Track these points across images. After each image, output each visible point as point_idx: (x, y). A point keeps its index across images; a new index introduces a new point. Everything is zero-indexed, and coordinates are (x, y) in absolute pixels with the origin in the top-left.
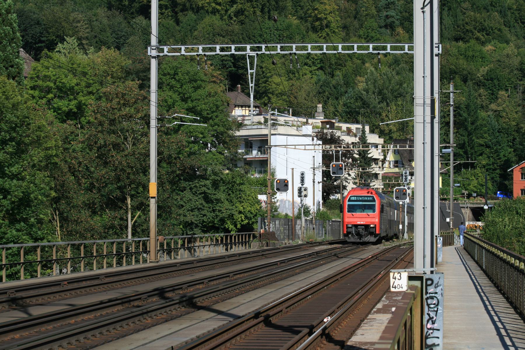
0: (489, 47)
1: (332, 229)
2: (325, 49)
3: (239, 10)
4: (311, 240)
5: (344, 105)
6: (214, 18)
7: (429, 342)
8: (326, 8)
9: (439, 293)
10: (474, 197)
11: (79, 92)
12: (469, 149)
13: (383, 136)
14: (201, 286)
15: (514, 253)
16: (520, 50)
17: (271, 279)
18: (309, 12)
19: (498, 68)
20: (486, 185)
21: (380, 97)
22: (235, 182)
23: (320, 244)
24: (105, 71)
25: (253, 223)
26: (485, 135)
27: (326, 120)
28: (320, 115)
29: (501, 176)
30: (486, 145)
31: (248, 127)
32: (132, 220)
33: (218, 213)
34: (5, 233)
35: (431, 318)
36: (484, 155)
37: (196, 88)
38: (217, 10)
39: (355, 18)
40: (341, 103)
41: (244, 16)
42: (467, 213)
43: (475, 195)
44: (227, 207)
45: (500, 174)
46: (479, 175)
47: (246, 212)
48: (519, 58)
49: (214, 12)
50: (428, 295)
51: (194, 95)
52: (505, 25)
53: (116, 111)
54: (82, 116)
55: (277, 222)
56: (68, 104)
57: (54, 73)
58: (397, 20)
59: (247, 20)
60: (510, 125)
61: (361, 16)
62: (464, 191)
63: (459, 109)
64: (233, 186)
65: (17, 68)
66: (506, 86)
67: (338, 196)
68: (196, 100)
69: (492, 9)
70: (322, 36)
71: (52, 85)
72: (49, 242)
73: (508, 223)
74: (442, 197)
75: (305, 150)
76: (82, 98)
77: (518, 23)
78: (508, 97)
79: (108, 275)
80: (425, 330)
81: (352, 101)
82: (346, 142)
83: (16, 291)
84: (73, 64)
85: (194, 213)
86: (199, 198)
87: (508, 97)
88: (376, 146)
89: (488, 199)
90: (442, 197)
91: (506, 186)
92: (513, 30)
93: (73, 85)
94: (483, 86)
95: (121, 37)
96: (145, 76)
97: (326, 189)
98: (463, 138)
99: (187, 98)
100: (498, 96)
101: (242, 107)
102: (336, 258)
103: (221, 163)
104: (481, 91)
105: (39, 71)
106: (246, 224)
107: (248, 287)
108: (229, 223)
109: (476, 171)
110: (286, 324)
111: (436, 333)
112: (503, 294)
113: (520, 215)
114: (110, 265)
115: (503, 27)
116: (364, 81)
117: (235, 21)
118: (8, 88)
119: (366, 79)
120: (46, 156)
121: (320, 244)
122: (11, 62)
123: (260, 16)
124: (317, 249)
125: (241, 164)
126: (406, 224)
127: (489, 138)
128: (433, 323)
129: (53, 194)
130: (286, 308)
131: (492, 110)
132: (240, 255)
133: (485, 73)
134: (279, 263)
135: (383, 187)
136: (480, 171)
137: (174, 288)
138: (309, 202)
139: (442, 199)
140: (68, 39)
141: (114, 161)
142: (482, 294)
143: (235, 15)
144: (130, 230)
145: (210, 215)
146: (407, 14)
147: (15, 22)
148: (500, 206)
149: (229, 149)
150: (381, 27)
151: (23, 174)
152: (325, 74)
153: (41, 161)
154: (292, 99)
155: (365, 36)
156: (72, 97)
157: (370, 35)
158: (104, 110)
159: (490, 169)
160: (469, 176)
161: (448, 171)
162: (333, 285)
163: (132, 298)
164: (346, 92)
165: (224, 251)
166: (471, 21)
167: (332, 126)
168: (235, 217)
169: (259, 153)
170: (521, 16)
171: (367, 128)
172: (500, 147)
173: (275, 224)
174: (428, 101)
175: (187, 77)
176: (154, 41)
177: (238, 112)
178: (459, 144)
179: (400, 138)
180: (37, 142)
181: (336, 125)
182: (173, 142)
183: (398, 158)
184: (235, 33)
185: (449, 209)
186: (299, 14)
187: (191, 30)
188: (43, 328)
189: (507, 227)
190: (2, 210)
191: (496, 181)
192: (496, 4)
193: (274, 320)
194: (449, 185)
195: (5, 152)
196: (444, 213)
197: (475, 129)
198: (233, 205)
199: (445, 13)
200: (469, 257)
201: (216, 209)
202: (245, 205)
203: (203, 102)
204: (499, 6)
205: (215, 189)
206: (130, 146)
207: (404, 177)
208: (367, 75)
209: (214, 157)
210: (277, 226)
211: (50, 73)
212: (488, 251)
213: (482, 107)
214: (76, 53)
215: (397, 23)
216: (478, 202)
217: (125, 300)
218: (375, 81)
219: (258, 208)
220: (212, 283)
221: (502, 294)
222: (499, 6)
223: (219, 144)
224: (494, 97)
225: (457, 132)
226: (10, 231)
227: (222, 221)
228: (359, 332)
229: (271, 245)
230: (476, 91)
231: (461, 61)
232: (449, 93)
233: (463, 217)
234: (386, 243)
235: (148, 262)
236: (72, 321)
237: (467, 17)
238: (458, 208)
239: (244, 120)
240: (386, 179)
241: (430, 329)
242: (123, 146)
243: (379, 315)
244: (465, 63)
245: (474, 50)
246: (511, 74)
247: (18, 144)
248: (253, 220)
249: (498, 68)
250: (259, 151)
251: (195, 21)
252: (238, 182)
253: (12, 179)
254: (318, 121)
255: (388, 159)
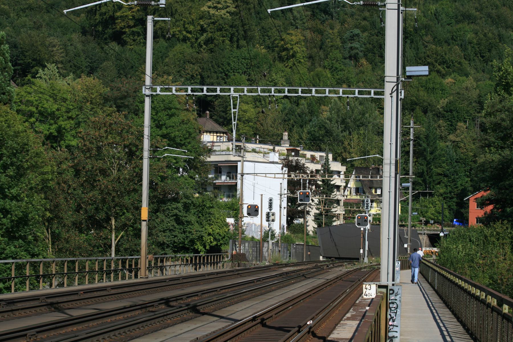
0: (449, 80)
1: (296, 252)
2: (300, 92)
3: (209, 39)
4: (277, 262)
5: (309, 133)
6: (185, 46)
7: (390, 334)
8: (292, 39)
9: (398, 300)
10: (432, 224)
11: (59, 117)
12: (427, 178)
13: (345, 164)
14: (196, 298)
15: (463, 277)
16: (479, 83)
17: (253, 294)
18: (277, 42)
19: (457, 100)
20: (443, 213)
21: (343, 126)
22: (205, 206)
23: (287, 265)
24: (84, 98)
25: (221, 244)
26: (443, 165)
27: (292, 148)
28: (286, 142)
29: (458, 204)
30: (444, 174)
31: (217, 153)
32: (115, 240)
33: (188, 235)
34: (4, 249)
35: (392, 318)
36: (441, 183)
37: (171, 116)
38: (188, 37)
39: (321, 48)
40: (306, 131)
41: (213, 45)
42: (424, 239)
43: (432, 222)
44: (197, 229)
45: (456, 203)
46: (437, 203)
47: (215, 234)
48: (478, 90)
49: (185, 40)
50: (390, 301)
51: (169, 122)
52: (465, 58)
53: (103, 139)
54: (62, 140)
55: (247, 245)
56: (49, 128)
57: (37, 98)
58: (361, 52)
59: (216, 49)
60: (467, 155)
61: (326, 46)
62: (421, 218)
63: (419, 139)
64: (203, 209)
65: (9, 95)
66: (465, 118)
67: (301, 220)
68: (170, 127)
69: (453, 43)
70: (288, 65)
71: (34, 109)
72: (44, 258)
73: (461, 249)
74: (400, 223)
75: (275, 178)
76: (62, 123)
77: (478, 57)
78: (466, 128)
79: (86, 291)
80: (388, 326)
81: (316, 129)
82: (311, 169)
83: (46, 298)
84: (53, 90)
85: (166, 234)
86: (171, 220)
87: (466, 128)
88: (338, 173)
89: (445, 226)
90: (400, 223)
91: (462, 214)
92: (473, 64)
93: (54, 110)
94: (443, 117)
95: (95, 62)
96: (122, 103)
97: (290, 214)
98: (422, 167)
99: (162, 125)
100: (457, 127)
101: (210, 132)
102: (304, 278)
103: (192, 187)
104: (441, 122)
105: (22, 96)
106: (214, 246)
107: (236, 300)
108: (199, 244)
109: (433, 199)
110: (277, 325)
111: (395, 329)
112: (450, 309)
113: (473, 242)
114: (61, 285)
115: (463, 60)
116: (328, 110)
117: (204, 49)
118: (9, 117)
119: (330, 109)
120: (42, 180)
121: (287, 265)
122: (3, 89)
123: (229, 46)
124: (285, 270)
125: (210, 188)
126: (367, 248)
127: (447, 167)
128: (393, 321)
129: (48, 214)
130: (275, 314)
131: (451, 141)
132: (209, 274)
133: (444, 105)
134: (255, 281)
135: (344, 213)
136: (437, 199)
137: (177, 298)
138: (276, 227)
139: (401, 226)
140: (48, 65)
141: (101, 185)
142: (432, 308)
143: (204, 44)
144: (113, 248)
145: (181, 236)
146: (371, 46)
147: (8, 53)
148: (454, 234)
149: (200, 174)
150: (345, 59)
151: (22, 196)
152: (290, 102)
153: (38, 185)
154: (258, 126)
155: (330, 67)
156: (52, 122)
157: (335, 66)
158: (93, 138)
159: (447, 197)
160: (427, 204)
161: (408, 199)
162: (307, 300)
163: (178, 298)
164: (310, 121)
165: (193, 270)
166: (433, 54)
167: (297, 154)
168: (204, 239)
169: (228, 178)
170: (481, 50)
171: (330, 156)
172: (457, 177)
173: (245, 246)
174: (393, 162)
175: (162, 105)
176: (148, 81)
177: (207, 138)
178: (419, 173)
179: (361, 166)
180: (34, 167)
181: (301, 152)
182: (155, 169)
183: (359, 185)
184: (205, 60)
185: (407, 235)
186: (267, 44)
187: (162, 57)
188: (91, 324)
189: (460, 253)
190: (2, 228)
191: (452, 209)
192: (457, 38)
193: (268, 323)
194: (407, 212)
195: (6, 176)
196: (402, 239)
197: (433, 159)
198: (203, 227)
199: (408, 45)
200: (424, 279)
201: (187, 231)
202: (214, 227)
203: (177, 129)
204: (460, 40)
205: (186, 212)
206: (116, 171)
207: (366, 205)
208: (331, 104)
209: (187, 181)
210: (247, 248)
211: (33, 98)
212: (439, 273)
213: (441, 137)
214: (56, 79)
215: (361, 54)
216: (434, 229)
217: (144, 306)
218: (339, 110)
219: (227, 230)
220: (204, 296)
221: (448, 308)
222: (460, 40)
223: (190, 169)
224: (452, 128)
225: (416, 162)
226: (9, 248)
227: (192, 242)
228: (335, 332)
229: (242, 265)
230: (435, 121)
231: (422, 93)
232: (410, 128)
233: (421, 243)
234: (347, 266)
235: (139, 277)
236: (109, 320)
237: (429, 50)
238: (415, 235)
239: (213, 146)
240: (348, 205)
241: (391, 325)
242: (109, 171)
243: (349, 321)
244: (426, 95)
245: (434, 83)
246: (470, 106)
247: (18, 168)
248: (221, 242)
249: (457, 100)
250: (228, 176)
251: (167, 48)
252: (208, 205)
253: (12, 200)
254: (284, 148)
255: (349, 186)
